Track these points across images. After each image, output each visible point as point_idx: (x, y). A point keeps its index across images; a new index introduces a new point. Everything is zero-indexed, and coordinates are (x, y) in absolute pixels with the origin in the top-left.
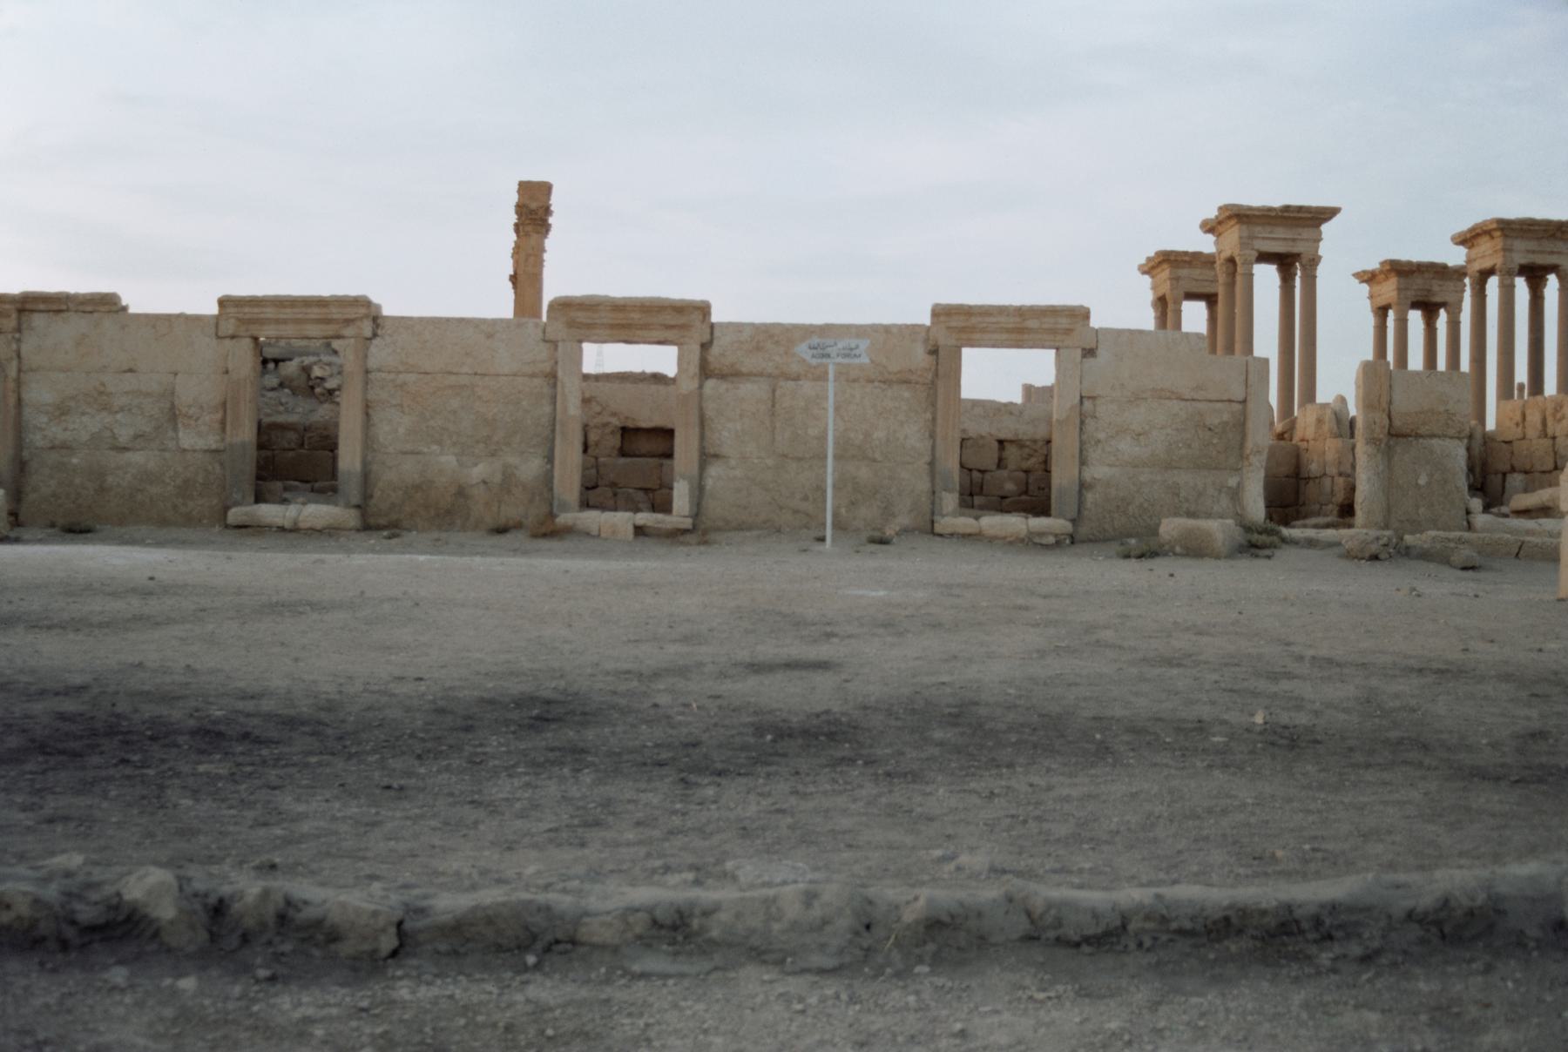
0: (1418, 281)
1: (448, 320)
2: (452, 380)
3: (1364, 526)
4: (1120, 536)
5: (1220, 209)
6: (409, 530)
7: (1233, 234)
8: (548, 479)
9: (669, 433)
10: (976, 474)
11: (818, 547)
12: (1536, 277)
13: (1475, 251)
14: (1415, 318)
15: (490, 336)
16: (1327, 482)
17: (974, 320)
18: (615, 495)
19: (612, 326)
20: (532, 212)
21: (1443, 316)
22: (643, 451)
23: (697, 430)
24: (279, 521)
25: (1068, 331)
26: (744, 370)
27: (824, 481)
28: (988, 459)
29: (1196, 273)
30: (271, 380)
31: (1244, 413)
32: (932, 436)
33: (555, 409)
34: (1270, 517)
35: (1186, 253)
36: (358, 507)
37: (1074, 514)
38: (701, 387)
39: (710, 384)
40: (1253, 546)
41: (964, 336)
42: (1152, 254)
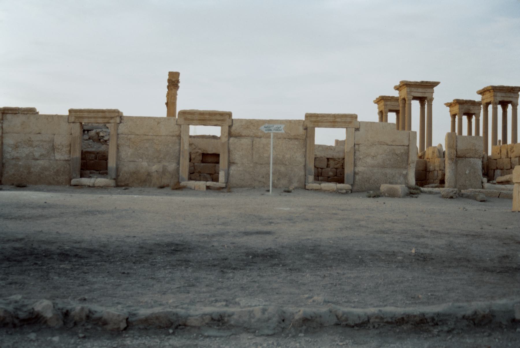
0: (466, 106)
1: (145, 118)
2: (146, 137)
3: (448, 187)
4: (367, 190)
5: (400, 82)
7: (405, 90)
8: (178, 170)
9: (218, 155)
10: (320, 170)
11: (267, 193)
12: (504, 104)
13: (484, 96)
14: (465, 118)
16: (436, 173)
17: (319, 119)
19: (200, 120)
20: (173, 82)
21: (474, 118)
22: (209, 161)
23: (227, 154)
24: (88, 184)
25: (350, 122)
26: (243, 135)
27: (269, 171)
28: (324, 164)
30: (86, 137)
31: (408, 149)
32: (305, 156)
33: (180, 148)
34: (417, 184)
35: (389, 97)
37: (352, 183)
39: (232, 139)
41: (316, 124)
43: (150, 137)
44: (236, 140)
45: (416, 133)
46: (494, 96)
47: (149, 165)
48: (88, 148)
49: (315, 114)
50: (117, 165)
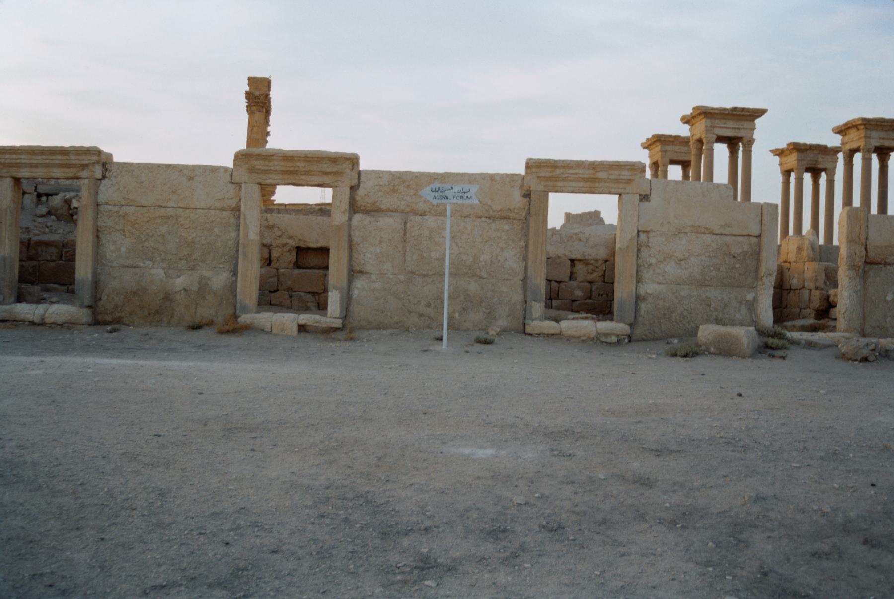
0: (810, 156)
1: (159, 166)
2: (162, 211)
3: (846, 331)
4: (665, 337)
5: (694, 109)
6: (128, 325)
7: (701, 125)
8: (232, 288)
9: (325, 251)
10: (554, 284)
11: (436, 347)
12: (883, 153)
13: (847, 137)
14: (807, 177)
15: (191, 179)
16: (806, 293)
17: (558, 172)
18: (291, 296)
20: (256, 97)
22: (312, 265)
24: (30, 317)
25: (629, 181)
26: (383, 207)
27: (442, 292)
29: (677, 148)
30: (43, 209)
31: (759, 245)
33: (239, 235)
34: (775, 322)
35: (671, 136)
37: (632, 320)
38: (350, 219)
39: (357, 217)
40: (767, 346)
42: (650, 136)
43: (170, 212)
44: (367, 219)
46: (867, 137)
47: (168, 276)
48: (45, 233)
49: (548, 161)
50: (95, 274)
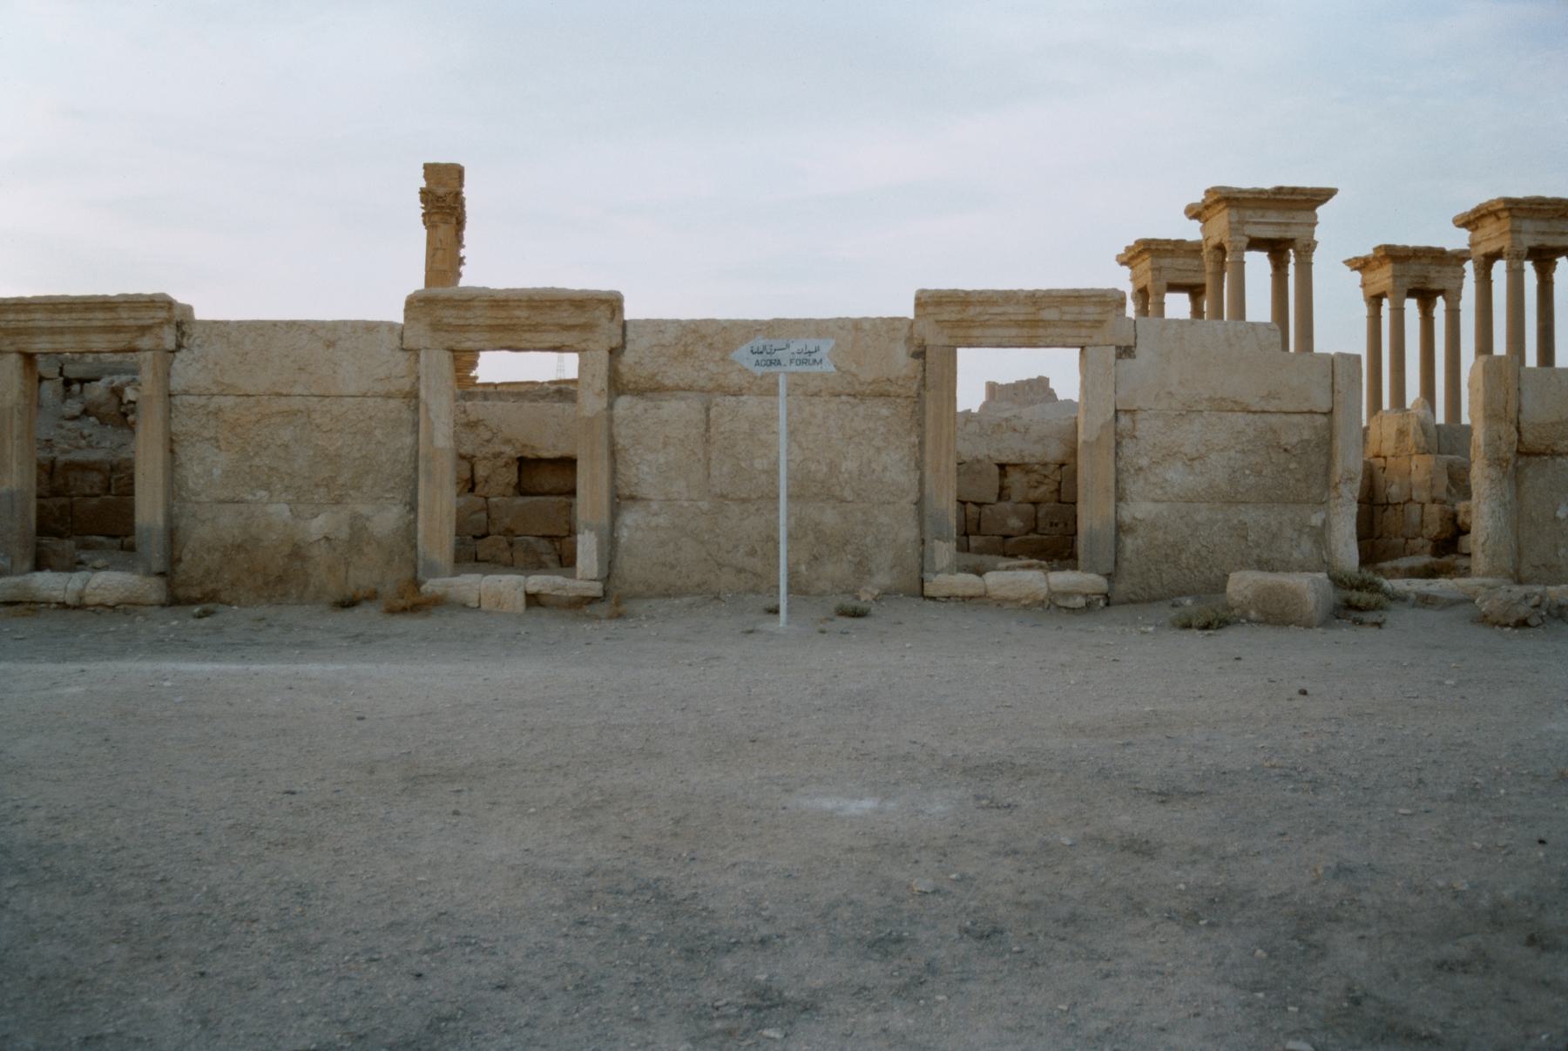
0: (1415, 268)
2: (283, 404)
3: (1485, 575)
4: (1171, 596)
5: (1207, 192)
8: (409, 534)
9: (568, 464)
10: (972, 509)
11: (768, 625)
12: (1544, 259)
13: (1479, 234)
14: (1411, 306)
15: (331, 344)
16: (1414, 510)
17: (971, 312)
18: (511, 545)
19: (492, 328)
20: (439, 198)
21: (1440, 307)
22: (547, 488)
23: (606, 463)
24: (58, 595)
25: (1098, 324)
26: (667, 382)
27: (777, 529)
28: (987, 489)
29: (1180, 262)
30: (74, 407)
31: (1330, 428)
33: (417, 441)
34: (1362, 563)
35: (1168, 242)
36: (162, 574)
37: (1110, 567)
38: (611, 406)
39: (623, 402)
40: (1350, 606)
41: (961, 333)
43: (296, 403)
44: (640, 405)
45: (1358, 358)
47: (296, 516)
48: (79, 448)
49: (955, 292)
50: (170, 517)
